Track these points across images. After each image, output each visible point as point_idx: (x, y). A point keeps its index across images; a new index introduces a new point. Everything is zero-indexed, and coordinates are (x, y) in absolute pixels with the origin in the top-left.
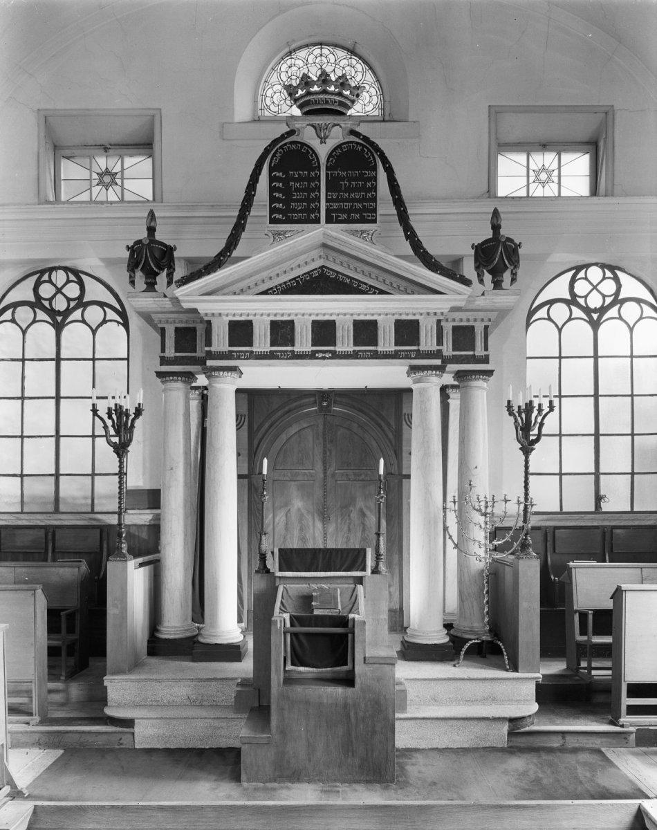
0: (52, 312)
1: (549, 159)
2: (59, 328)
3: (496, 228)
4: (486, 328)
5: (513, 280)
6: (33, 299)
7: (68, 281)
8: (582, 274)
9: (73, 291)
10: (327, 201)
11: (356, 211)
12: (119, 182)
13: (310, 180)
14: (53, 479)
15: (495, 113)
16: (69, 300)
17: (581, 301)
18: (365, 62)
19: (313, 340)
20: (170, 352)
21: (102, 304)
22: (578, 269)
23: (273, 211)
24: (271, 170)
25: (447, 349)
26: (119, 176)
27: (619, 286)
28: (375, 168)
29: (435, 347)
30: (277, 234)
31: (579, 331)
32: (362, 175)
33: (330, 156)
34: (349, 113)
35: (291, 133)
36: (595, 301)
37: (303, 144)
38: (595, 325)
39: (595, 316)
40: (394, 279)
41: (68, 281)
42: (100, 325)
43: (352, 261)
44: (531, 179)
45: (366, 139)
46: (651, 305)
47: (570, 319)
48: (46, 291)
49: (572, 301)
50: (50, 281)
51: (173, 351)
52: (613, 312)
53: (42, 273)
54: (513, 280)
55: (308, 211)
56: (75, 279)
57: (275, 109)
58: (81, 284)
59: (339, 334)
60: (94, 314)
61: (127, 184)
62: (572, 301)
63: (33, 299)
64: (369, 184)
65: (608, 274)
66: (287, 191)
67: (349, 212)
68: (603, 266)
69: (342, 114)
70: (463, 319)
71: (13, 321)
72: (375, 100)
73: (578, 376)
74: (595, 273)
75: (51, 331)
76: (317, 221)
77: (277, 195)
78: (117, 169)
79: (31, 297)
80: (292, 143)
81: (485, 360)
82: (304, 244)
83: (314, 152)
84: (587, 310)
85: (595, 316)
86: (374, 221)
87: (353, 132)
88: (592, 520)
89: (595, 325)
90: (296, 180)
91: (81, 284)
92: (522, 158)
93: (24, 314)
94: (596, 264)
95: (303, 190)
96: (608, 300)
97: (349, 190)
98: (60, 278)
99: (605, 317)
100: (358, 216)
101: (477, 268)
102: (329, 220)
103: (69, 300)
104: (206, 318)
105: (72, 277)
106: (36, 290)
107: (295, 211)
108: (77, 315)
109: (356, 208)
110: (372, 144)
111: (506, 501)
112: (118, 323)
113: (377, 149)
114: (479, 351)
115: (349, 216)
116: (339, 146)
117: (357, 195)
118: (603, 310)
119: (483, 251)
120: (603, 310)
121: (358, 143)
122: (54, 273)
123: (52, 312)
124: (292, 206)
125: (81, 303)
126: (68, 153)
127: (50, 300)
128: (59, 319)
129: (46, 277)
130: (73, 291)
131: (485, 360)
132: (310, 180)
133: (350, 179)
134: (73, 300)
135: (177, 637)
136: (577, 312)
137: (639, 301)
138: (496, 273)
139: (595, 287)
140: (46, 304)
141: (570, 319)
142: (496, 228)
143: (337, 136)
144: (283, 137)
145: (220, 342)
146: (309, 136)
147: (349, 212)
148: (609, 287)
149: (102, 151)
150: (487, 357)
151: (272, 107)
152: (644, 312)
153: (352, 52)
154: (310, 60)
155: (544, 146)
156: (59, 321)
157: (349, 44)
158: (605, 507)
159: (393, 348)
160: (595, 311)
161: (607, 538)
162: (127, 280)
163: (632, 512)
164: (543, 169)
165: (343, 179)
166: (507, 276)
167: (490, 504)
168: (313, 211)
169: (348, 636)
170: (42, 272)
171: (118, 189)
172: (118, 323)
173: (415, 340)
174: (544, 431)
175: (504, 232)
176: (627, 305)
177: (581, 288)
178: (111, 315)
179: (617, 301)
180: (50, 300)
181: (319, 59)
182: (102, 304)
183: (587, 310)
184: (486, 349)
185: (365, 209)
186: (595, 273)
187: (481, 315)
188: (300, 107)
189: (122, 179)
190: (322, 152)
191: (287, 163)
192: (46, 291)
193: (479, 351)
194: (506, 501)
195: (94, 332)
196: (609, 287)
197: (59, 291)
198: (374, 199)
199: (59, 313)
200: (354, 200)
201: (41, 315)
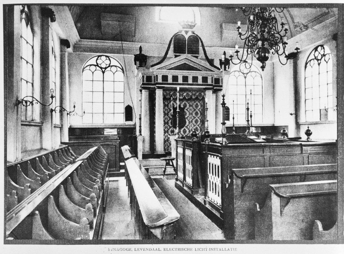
5: (229, 68)
8: (100, 58)
9: (108, 62)
17: (100, 65)
25: (214, 84)
31: (99, 73)
36: (103, 66)
39: (103, 70)
48: (99, 62)
51: (182, 81)
52: (109, 69)
54: (229, 68)
58: (110, 60)
62: (97, 65)
74: (104, 58)
76: (185, 53)
84: (101, 68)
89: (103, 72)
91: (110, 60)
93: (93, 68)
96: (107, 66)
99: (106, 70)
102: (188, 53)
113: (200, 38)
114: (221, 84)
118: (106, 68)
120: (106, 68)
145: (160, 80)
156: (103, 70)
159: (172, 82)
161: (182, 158)
169: (335, 179)
173: (197, 81)
184: (222, 84)
193: (221, 84)
201: (98, 68)
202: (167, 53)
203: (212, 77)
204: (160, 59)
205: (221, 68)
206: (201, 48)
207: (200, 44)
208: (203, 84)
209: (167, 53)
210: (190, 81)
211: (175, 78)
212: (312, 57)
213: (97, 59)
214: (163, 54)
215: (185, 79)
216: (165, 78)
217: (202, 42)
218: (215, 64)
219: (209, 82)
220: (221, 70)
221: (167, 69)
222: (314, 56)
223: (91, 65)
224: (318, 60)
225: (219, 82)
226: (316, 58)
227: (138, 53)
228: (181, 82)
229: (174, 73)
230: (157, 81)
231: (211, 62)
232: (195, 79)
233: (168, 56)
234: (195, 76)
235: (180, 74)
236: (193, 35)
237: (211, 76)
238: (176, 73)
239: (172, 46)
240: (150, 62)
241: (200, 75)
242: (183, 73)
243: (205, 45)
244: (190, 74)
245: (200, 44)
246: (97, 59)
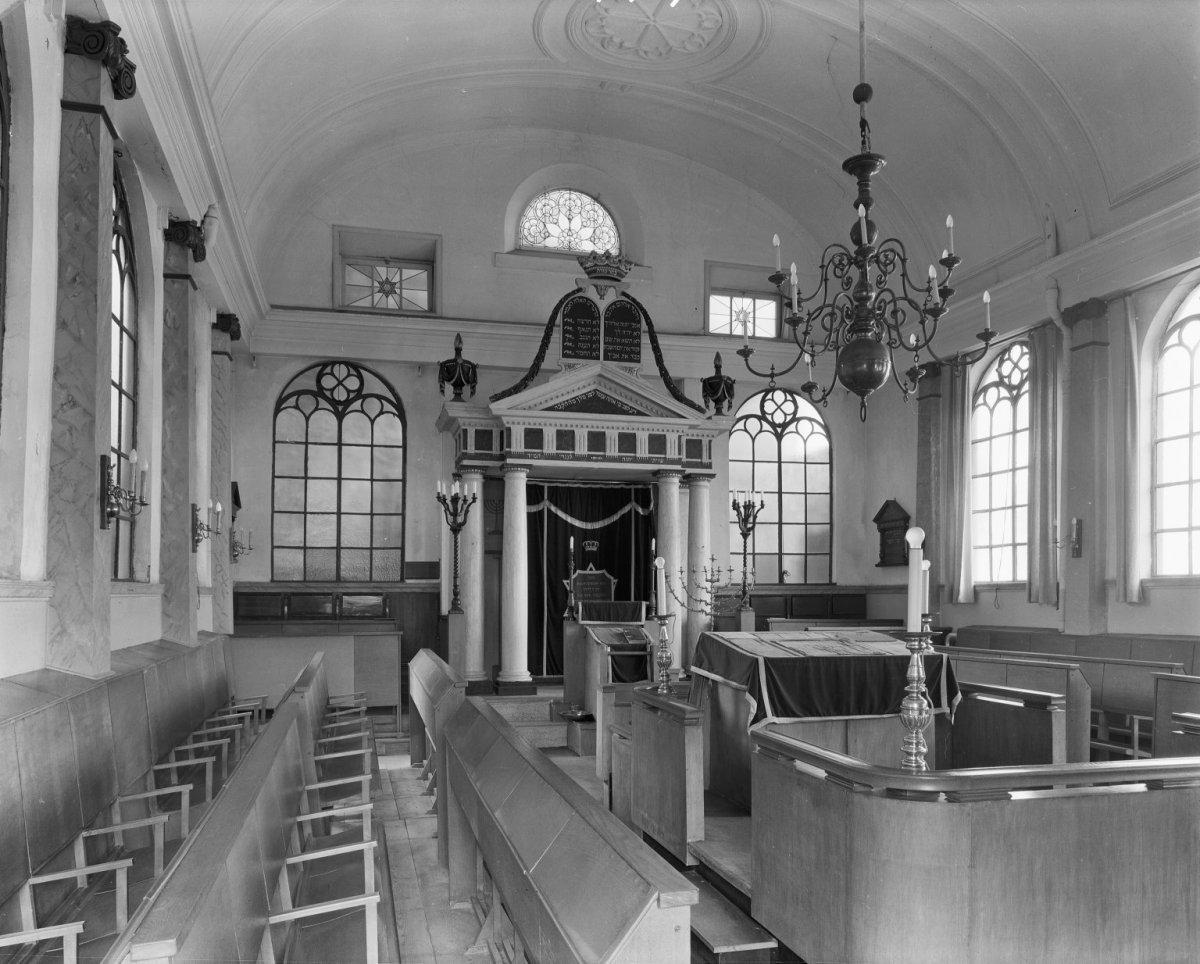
0: (334, 402)
1: (746, 303)
2: (340, 417)
3: (718, 368)
4: (710, 442)
5: (473, 393)
6: (315, 389)
7: (349, 375)
9: (353, 383)
10: (605, 343)
11: (626, 353)
12: (398, 291)
13: (593, 326)
14: (334, 551)
15: (709, 266)
16: (349, 391)
17: (769, 417)
18: (606, 208)
19: (589, 446)
20: (471, 449)
21: (380, 397)
22: (767, 392)
23: (565, 348)
24: (564, 316)
26: (398, 285)
27: (796, 407)
28: (639, 322)
29: (676, 456)
30: (570, 367)
31: (767, 440)
32: (631, 326)
33: (608, 310)
34: (623, 280)
35: (579, 290)
36: (779, 418)
37: (587, 299)
38: (779, 437)
39: (779, 430)
40: (637, 397)
41: (349, 375)
42: (378, 415)
43: (618, 387)
44: (734, 318)
45: (634, 300)
46: (819, 423)
47: (761, 431)
48: (328, 382)
49: (762, 417)
50: (332, 374)
51: (523, 446)
53: (325, 365)
54: (473, 393)
55: (591, 349)
56: (355, 373)
57: (532, 240)
58: (794, 402)
59: (608, 442)
60: (373, 406)
61: (405, 293)
62: (762, 417)
63: (315, 389)
64: (635, 333)
65: (789, 397)
66: (575, 334)
67: (621, 352)
68: (785, 391)
69: (619, 281)
70: (694, 435)
71: (297, 407)
72: (613, 240)
73: (766, 474)
75: (333, 420)
76: (598, 358)
77: (567, 335)
78: (396, 279)
79: (312, 385)
80: (580, 297)
81: (709, 466)
82: (582, 377)
83: (596, 306)
84: (773, 425)
85: (779, 430)
86: (639, 361)
87: (624, 294)
88: (778, 590)
90: (581, 325)
92: (726, 300)
93: (307, 402)
94: (780, 389)
95: (588, 334)
96: (789, 418)
97: (621, 336)
98: (341, 371)
100: (626, 356)
101: (704, 397)
103: (349, 391)
104: (507, 425)
105: (352, 372)
106: (318, 381)
107: (581, 349)
108: (357, 405)
109: (627, 352)
110: (638, 304)
111: (731, 571)
112: (394, 414)
113: (642, 309)
114: (496, 451)
115: (621, 356)
116: (614, 303)
117: (626, 341)
119: (710, 385)
120: (785, 425)
121: (628, 303)
122: (337, 366)
123: (334, 402)
124: (579, 347)
125: (360, 394)
126: (351, 261)
127: (332, 390)
128: (340, 408)
129: (328, 370)
130: (353, 383)
131: (709, 466)
132: (593, 326)
133: (622, 328)
134: (353, 391)
135: (477, 679)
136: (766, 426)
137: (811, 420)
138: (718, 402)
139: (779, 405)
140: (328, 394)
141: (761, 431)
142: (718, 368)
143: (611, 296)
144: (574, 292)
145: (518, 444)
146: (591, 293)
147: (621, 352)
148: (789, 408)
149: (383, 263)
150: (711, 463)
151: (529, 238)
152: (799, 410)
153: (596, 199)
154: (561, 202)
155: (743, 293)
156: (340, 410)
157: (594, 194)
158: (787, 580)
159: (647, 455)
160: (779, 425)
162: (439, 390)
163: (805, 584)
164: (742, 311)
165: (616, 327)
166: (725, 404)
167: (716, 573)
168: (595, 350)
170: (325, 365)
171: (397, 297)
172: (394, 414)
174: (757, 520)
175: (724, 372)
176: (802, 422)
177: (769, 407)
178: (388, 407)
179: (795, 419)
180: (332, 390)
181: (568, 202)
182: (380, 397)
183: (773, 425)
184: (502, 448)
185: (632, 352)
186: (779, 396)
187: (707, 432)
188: (588, 273)
189: (401, 288)
190: (603, 305)
191: (576, 314)
192: (328, 382)
193: (705, 460)
194: (731, 571)
195: (372, 422)
196: (789, 408)
197: (340, 383)
198: (639, 345)
199: (339, 403)
200: (623, 344)
201: (323, 403)
202: (540, 357)
203: (680, 437)
204: (523, 375)
205: (708, 407)
206: (645, 340)
207: (644, 326)
208: (650, 458)
209: (540, 357)
210: (581, 447)
211: (566, 439)
212: (992, 377)
213: (763, 401)
214: (529, 364)
215: (597, 440)
216: (534, 437)
217: (649, 323)
218: (688, 395)
219: (672, 452)
220: (708, 414)
221: (542, 407)
222: (997, 374)
223: (747, 417)
224: (1010, 388)
225: (701, 450)
226: (1006, 380)
227: (712, 373)
228: (616, 454)
229: (564, 422)
230: (509, 446)
231: (675, 389)
232: (628, 442)
233: (544, 366)
234: (654, 433)
235: (583, 425)
236: (624, 298)
237: (677, 430)
238: (569, 422)
239: (557, 337)
240: (485, 385)
241: (642, 430)
242: (558, 422)
243: (656, 328)
244: (612, 426)
245: (644, 326)
246: (763, 401)
